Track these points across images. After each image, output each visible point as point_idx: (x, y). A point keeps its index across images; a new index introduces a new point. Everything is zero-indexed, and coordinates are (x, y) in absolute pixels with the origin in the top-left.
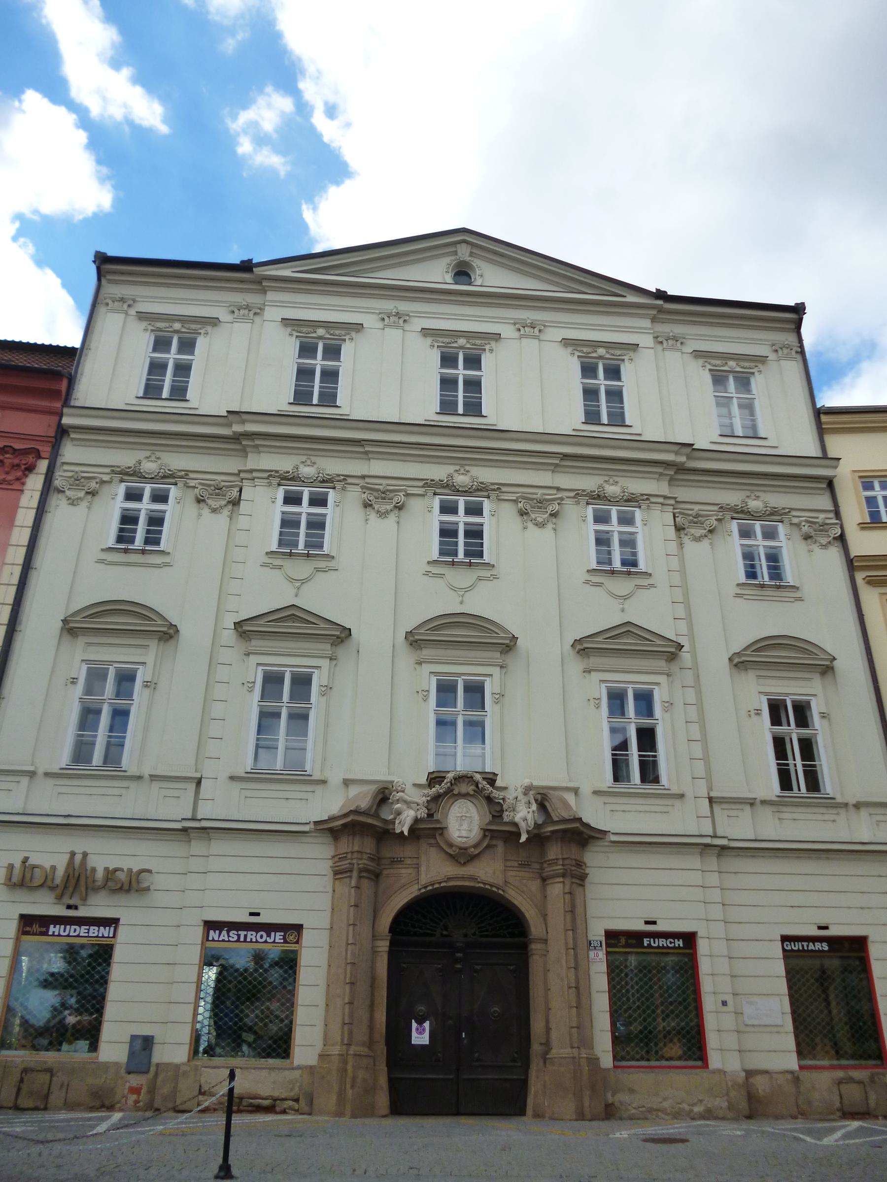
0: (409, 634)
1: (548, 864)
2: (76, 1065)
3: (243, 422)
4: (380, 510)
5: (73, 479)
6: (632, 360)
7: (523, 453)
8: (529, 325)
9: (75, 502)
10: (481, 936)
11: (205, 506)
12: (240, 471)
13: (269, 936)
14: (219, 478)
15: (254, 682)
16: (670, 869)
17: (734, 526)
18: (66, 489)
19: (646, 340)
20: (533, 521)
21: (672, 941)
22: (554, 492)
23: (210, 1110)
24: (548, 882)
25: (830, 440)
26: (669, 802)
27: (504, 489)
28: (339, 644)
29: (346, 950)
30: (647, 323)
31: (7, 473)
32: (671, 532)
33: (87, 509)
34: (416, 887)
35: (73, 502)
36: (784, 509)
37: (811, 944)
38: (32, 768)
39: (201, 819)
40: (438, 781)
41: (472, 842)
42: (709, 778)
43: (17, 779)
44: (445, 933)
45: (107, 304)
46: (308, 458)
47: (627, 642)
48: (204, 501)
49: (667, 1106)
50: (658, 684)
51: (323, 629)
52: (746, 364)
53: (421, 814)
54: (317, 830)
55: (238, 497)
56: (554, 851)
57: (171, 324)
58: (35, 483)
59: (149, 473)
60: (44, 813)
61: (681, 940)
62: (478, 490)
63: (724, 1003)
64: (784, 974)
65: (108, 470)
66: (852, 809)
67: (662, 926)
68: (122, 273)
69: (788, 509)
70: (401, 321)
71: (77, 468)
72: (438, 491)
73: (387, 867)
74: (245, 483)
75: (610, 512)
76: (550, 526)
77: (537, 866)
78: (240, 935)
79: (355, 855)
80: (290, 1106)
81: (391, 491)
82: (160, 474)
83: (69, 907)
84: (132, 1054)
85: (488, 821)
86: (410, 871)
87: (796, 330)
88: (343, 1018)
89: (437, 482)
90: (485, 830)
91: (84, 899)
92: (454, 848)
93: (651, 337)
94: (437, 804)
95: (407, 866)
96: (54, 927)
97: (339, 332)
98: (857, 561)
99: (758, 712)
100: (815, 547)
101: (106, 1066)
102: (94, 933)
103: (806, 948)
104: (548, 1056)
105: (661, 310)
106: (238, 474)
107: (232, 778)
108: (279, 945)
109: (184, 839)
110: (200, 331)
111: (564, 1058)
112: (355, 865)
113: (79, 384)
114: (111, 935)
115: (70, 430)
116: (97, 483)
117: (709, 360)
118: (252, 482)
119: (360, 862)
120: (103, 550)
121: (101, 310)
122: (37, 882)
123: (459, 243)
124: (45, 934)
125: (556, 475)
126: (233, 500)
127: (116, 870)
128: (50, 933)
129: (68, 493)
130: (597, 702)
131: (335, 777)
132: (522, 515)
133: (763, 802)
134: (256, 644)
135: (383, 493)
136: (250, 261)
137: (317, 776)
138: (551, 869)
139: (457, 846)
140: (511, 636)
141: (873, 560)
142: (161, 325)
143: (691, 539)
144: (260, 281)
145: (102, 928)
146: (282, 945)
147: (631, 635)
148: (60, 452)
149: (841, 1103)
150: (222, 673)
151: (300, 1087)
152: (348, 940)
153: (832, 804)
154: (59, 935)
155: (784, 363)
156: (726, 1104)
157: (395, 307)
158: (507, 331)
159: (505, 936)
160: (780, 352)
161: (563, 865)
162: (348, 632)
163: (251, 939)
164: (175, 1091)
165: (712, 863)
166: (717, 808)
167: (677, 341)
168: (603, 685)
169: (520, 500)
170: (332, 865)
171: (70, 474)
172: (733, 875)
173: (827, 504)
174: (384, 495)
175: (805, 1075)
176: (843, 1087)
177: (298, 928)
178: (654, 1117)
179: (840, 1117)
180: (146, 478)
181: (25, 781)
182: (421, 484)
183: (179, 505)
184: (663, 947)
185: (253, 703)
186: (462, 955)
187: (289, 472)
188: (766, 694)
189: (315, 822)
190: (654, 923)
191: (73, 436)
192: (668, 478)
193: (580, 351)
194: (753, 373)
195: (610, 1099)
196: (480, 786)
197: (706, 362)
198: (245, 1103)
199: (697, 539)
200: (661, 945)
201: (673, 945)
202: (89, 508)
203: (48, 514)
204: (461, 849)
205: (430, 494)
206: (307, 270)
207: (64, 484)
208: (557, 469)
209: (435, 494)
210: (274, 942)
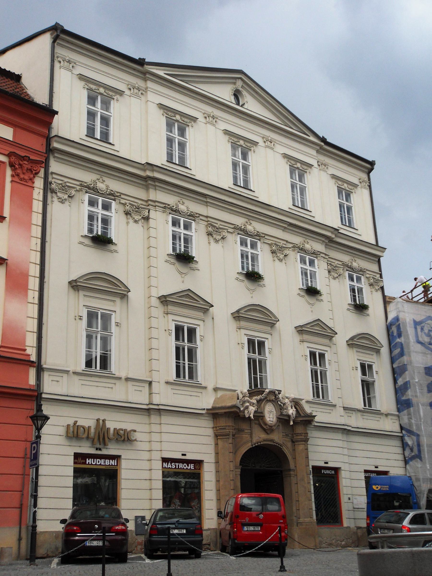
3: (153, 171)
4: (216, 238)
5: (61, 186)
7: (257, 213)
11: (131, 218)
13: (188, 466)
14: (140, 202)
17: (86, 197)
22: (285, 243)
30: (314, 153)
35: (62, 201)
43: (61, 374)
45: (60, 62)
46: (181, 199)
50: (327, 351)
58: (39, 183)
59: (101, 191)
60: (73, 396)
63: (349, 499)
65: (78, 183)
68: (68, 42)
71: (66, 180)
74: (150, 207)
77: (290, 435)
83: (97, 449)
86: (247, 436)
95: (246, 433)
96: (89, 460)
100: (373, 290)
105: (321, 147)
106: (147, 201)
107: (167, 383)
109: (146, 414)
110: (113, 97)
112: (231, 432)
114: (116, 464)
118: (154, 208)
119: (233, 431)
124: (85, 463)
128: (87, 463)
136: (144, 59)
137: (203, 385)
139: (269, 425)
142: (93, 87)
144: (145, 73)
163: (181, 467)
165: (345, 437)
169: (274, 245)
171: (60, 182)
174: (218, 230)
182: (232, 226)
185: (172, 343)
188: (359, 360)
189: (207, 409)
193: (290, 162)
204: (270, 426)
205: (236, 233)
206: (169, 74)
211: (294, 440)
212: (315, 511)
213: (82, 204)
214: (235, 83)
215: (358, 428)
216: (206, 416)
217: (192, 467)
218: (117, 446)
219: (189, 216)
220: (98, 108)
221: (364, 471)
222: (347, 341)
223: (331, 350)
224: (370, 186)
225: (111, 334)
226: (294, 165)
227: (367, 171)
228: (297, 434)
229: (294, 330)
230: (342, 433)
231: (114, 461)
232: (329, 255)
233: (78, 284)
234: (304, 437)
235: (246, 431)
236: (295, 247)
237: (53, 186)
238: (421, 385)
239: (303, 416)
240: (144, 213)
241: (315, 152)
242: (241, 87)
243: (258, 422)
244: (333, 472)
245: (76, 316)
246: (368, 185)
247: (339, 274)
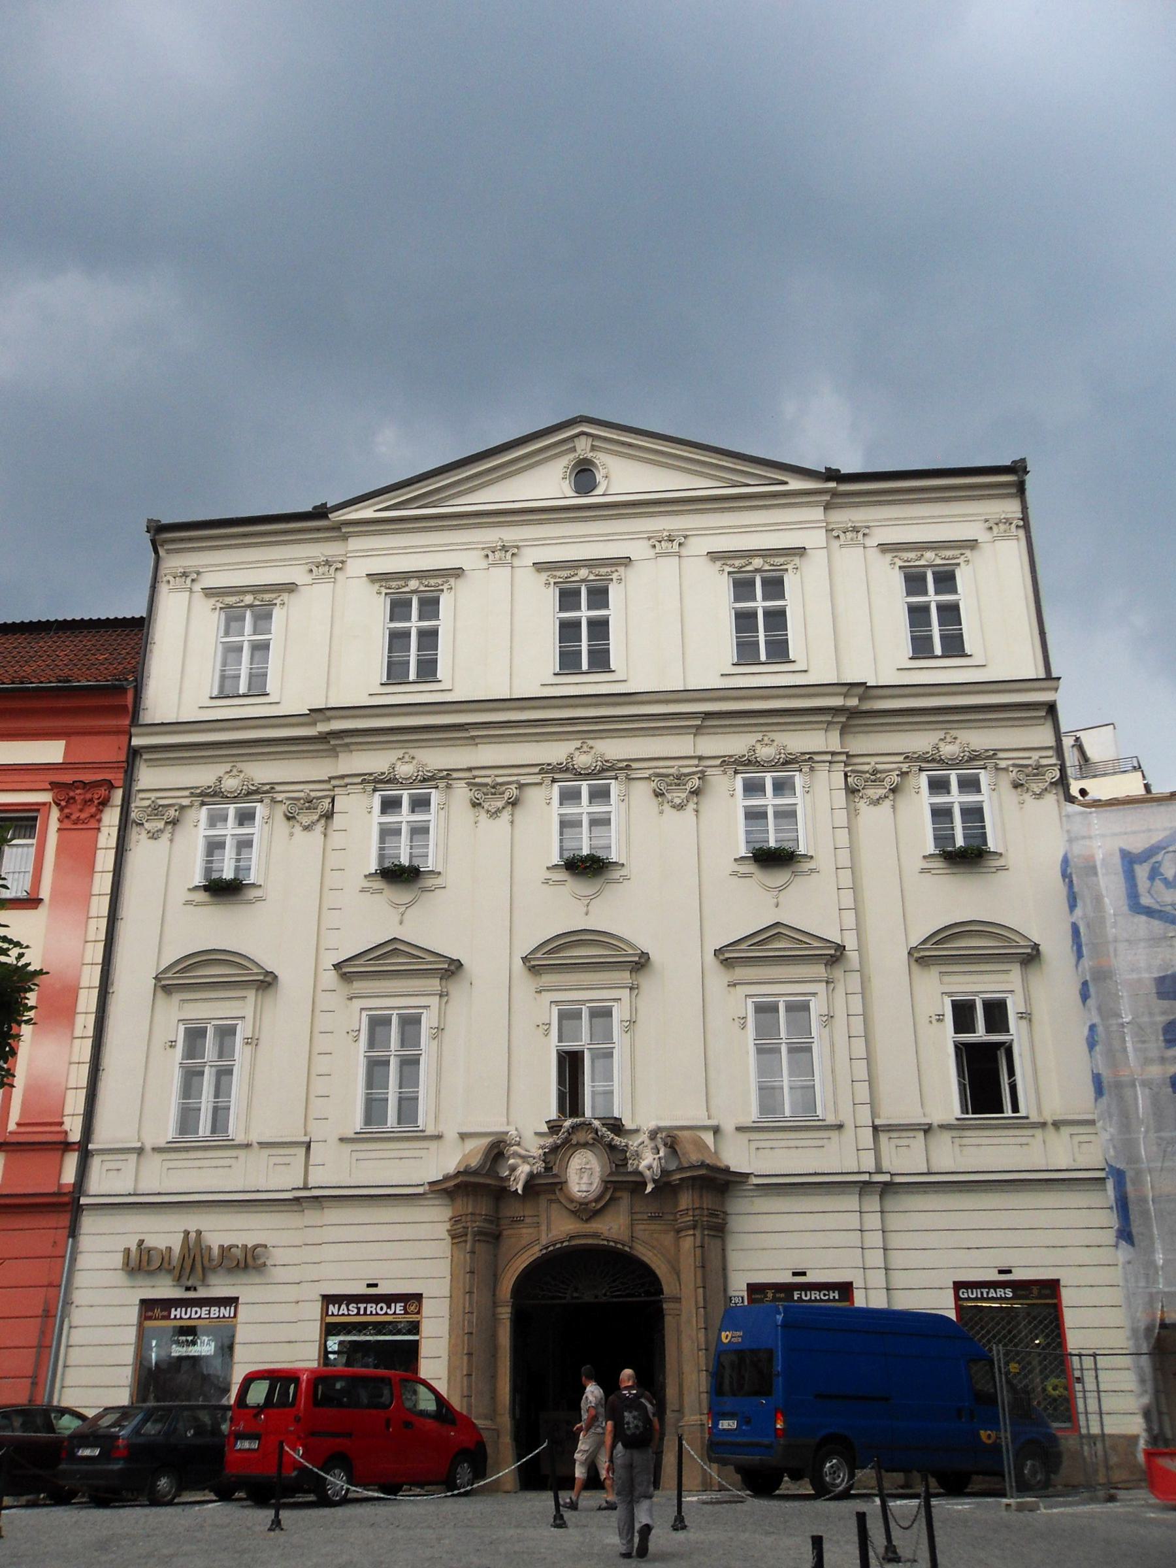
0: (525, 959)
4: (490, 809)
5: (150, 809)
7: (655, 717)
8: (666, 538)
12: (331, 778)
13: (389, 1307)
15: (359, 1030)
17: (923, 780)
18: (144, 821)
19: (814, 539)
20: (670, 804)
21: (827, 1293)
22: (696, 762)
28: (450, 976)
30: (817, 513)
31: (81, 811)
32: (841, 797)
33: (169, 842)
34: (537, 1248)
35: (154, 836)
37: (992, 1290)
38: (139, 1145)
39: (311, 1188)
41: (591, 1197)
42: (873, 1104)
44: (575, 1295)
50: (814, 994)
51: (430, 963)
54: (433, 1192)
56: (685, 1200)
58: (111, 818)
61: (836, 1292)
66: (1051, 1129)
67: (812, 1278)
69: (992, 750)
70: (860, 535)
71: (153, 795)
72: (557, 776)
73: (506, 1227)
74: (337, 791)
79: (469, 1218)
81: (502, 784)
83: (188, 1289)
86: (530, 1230)
87: (1019, 494)
88: (462, 1391)
89: (555, 766)
90: (606, 1182)
96: (176, 1310)
97: (436, 581)
100: (1027, 797)
103: (985, 1296)
105: (834, 494)
107: (342, 1140)
108: (400, 1316)
111: (693, 1425)
114: (232, 1315)
115: (141, 751)
116: (176, 810)
117: (899, 554)
119: (474, 1225)
122: (156, 1264)
123: (577, 436)
124: (168, 1317)
125: (700, 739)
127: (230, 1247)
128: (172, 1316)
129: (147, 825)
130: (742, 1021)
131: (451, 1134)
133: (941, 1127)
134: (359, 986)
135: (493, 787)
139: (577, 1202)
142: (231, 600)
144: (338, 527)
148: (135, 777)
150: (324, 1021)
152: (464, 1308)
158: (638, 550)
159: (640, 1296)
160: (995, 528)
161: (694, 1216)
162: (458, 965)
163: (371, 1312)
166: (883, 1138)
167: (858, 532)
169: (653, 779)
170: (449, 1228)
171: (147, 803)
174: (495, 789)
177: (418, 1297)
180: (581, 774)
181: (134, 1157)
182: (537, 770)
183: (994, 793)
184: (816, 1300)
188: (949, 994)
189: (429, 1183)
190: (804, 1274)
192: (840, 725)
194: (958, 564)
196: (599, 1133)
197: (896, 557)
200: (813, 1298)
201: (827, 1297)
202: (171, 840)
204: (581, 1204)
210: (395, 1313)
214: (574, 449)
217: (398, 1308)
218: (229, 1280)
219: (783, 764)
227: (1014, 491)
236: (551, 772)
238: (1140, 1028)
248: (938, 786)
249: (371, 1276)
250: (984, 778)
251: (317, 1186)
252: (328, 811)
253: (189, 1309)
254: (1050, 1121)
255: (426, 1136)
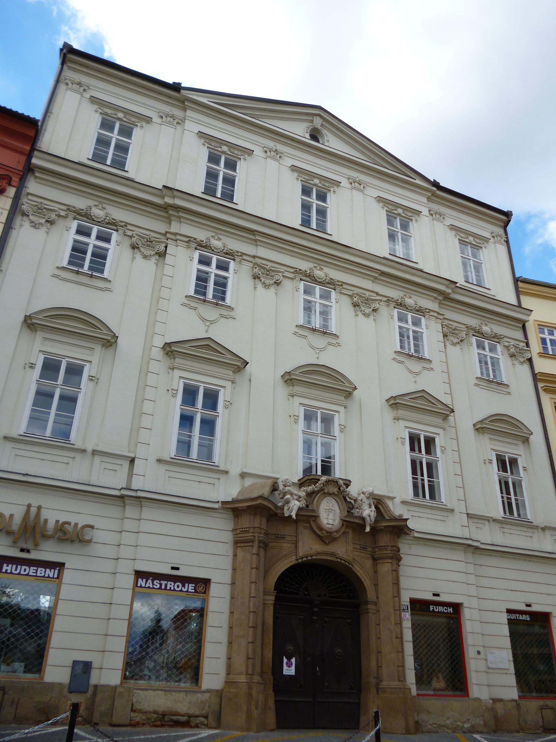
1: (379, 549)
2: (25, 685)
3: (174, 197)
5: (36, 208)
6: (246, 159)
7: (375, 270)
8: (358, 181)
9: (37, 226)
10: (330, 597)
13: (184, 586)
16: (447, 559)
17: (74, 225)
18: (30, 214)
19: (425, 211)
21: (447, 608)
22: (375, 295)
23: (139, 724)
24: (378, 562)
25: (523, 298)
26: (445, 514)
27: (345, 286)
29: (249, 602)
30: (425, 200)
33: (46, 234)
35: (35, 226)
36: (501, 335)
37: (521, 615)
40: (313, 482)
41: (335, 528)
44: (306, 593)
45: (67, 84)
47: (420, 404)
48: (138, 248)
49: (449, 723)
50: (438, 434)
52: (478, 241)
53: (303, 504)
54: (223, 508)
55: (164, 251)
57: (116, 113)
62: (328, 283)
63: (479, 653)
64: (508, 634)
66: (540, 530)
68: (81, 65)
70: (278, 156)
74: (169, 242)
75: (212, 258)
76: (372, 317)
77: (370, 550)
78: (162, 583)
80: (201, 722)
81: (273, 271)
82: (106, 220)
83: (22, 550)
84: (73, 676)
85: (345, 515)
86: (289, 545)
87: (504, 227)
89: (303, 272)
91: (36, 545)
92: (323, 532)
93: (427, 210)
94: (311, 498)
96: (8, 566)
98: (539, 375)
99: (490, 462)
100: (516, 362)
101: (52, 685)
102: (41, 573)
104: (379, 687)
105: (434, 194)
107: (159, 461)
109: (120, 504)
110: (137, 124)
113: (43, 137)
115: (36, 169)
120: (57, 268)
121: (62, 87)
126: (160, 252)
128: (4, 570)
131: (235, 471)
132: (355, 306)
136: (179, 84)
137: (222, 468)
138: (382, 552)
139: (325, 530)
140: (354, 387)
141: (546, 377)
142: (109, 111)
143: (450, 344)
145: (48, 570)
146: (194, 594)
147: (423, 399)
149: (543, 722)
150: (151, 379)
151: (209, 706)
152: (250, 593)
153: (529, 526)
154: (11, 573)
155: (498, 245)
156: (482, 722)
157: (275, 145)
163: (170, 588)
164: (112, 708)
165: (470, 558)
168: (407, 430)
169: (355, 296)
172: (479, 566)
173: (521, 337)
174: (269, 272)
175: (523, 702)
176: (544, 711)
177: (206, 582)
178: (442, 731)
179: (542, 731)
182: (292, 270)
183: (118, 247)
186: (317, 610)
187: (203, 242)
189: (222, 502)
191: (37, 174)
193: (387, 207)
195: (416, 719)
196: (342, 489)
198: (166, 718)
199: (454, 344)
200: (440, 611)
203: (14, 231)
204: (328, 532)
205: (298, 279)
207: (29, 209)
208: (375, 281)
209: (301, 280)
210: (187, 591)
211: (376, 556)
212: (413, 672)
213: (66, 232)
214: (312, 121)
215: (493, 545)
216: (221, 513)
217: (190, 588)
220: (115, 136)
221: (505, 611)
222: (474, 425)
223: (445, 434)
224: (507, 242)
225: (79, 390)
226: (393, 210)
228: (381, 548)
229: (386, 405)
230: (465, 551)
231: (53, 570)
232: (443, 315)
233: (34, 321)
234: (390, 552)
235: (289, 538)
237: (25, 207)
239: (387, 520)
240: (159, 247)
241: (426, 199)
242: (321, 126)
243: (309, 526)
244: (450, 610)
245: (26, 364)
246: (504, 241)
247: (460, 339)
248: (82, 231)
249: (176, 562)
250: (115, 236)
251: (546, 551)
252: (162, 251)
253: (19, 567)
254: (90, 449)
255: (220, 470)
